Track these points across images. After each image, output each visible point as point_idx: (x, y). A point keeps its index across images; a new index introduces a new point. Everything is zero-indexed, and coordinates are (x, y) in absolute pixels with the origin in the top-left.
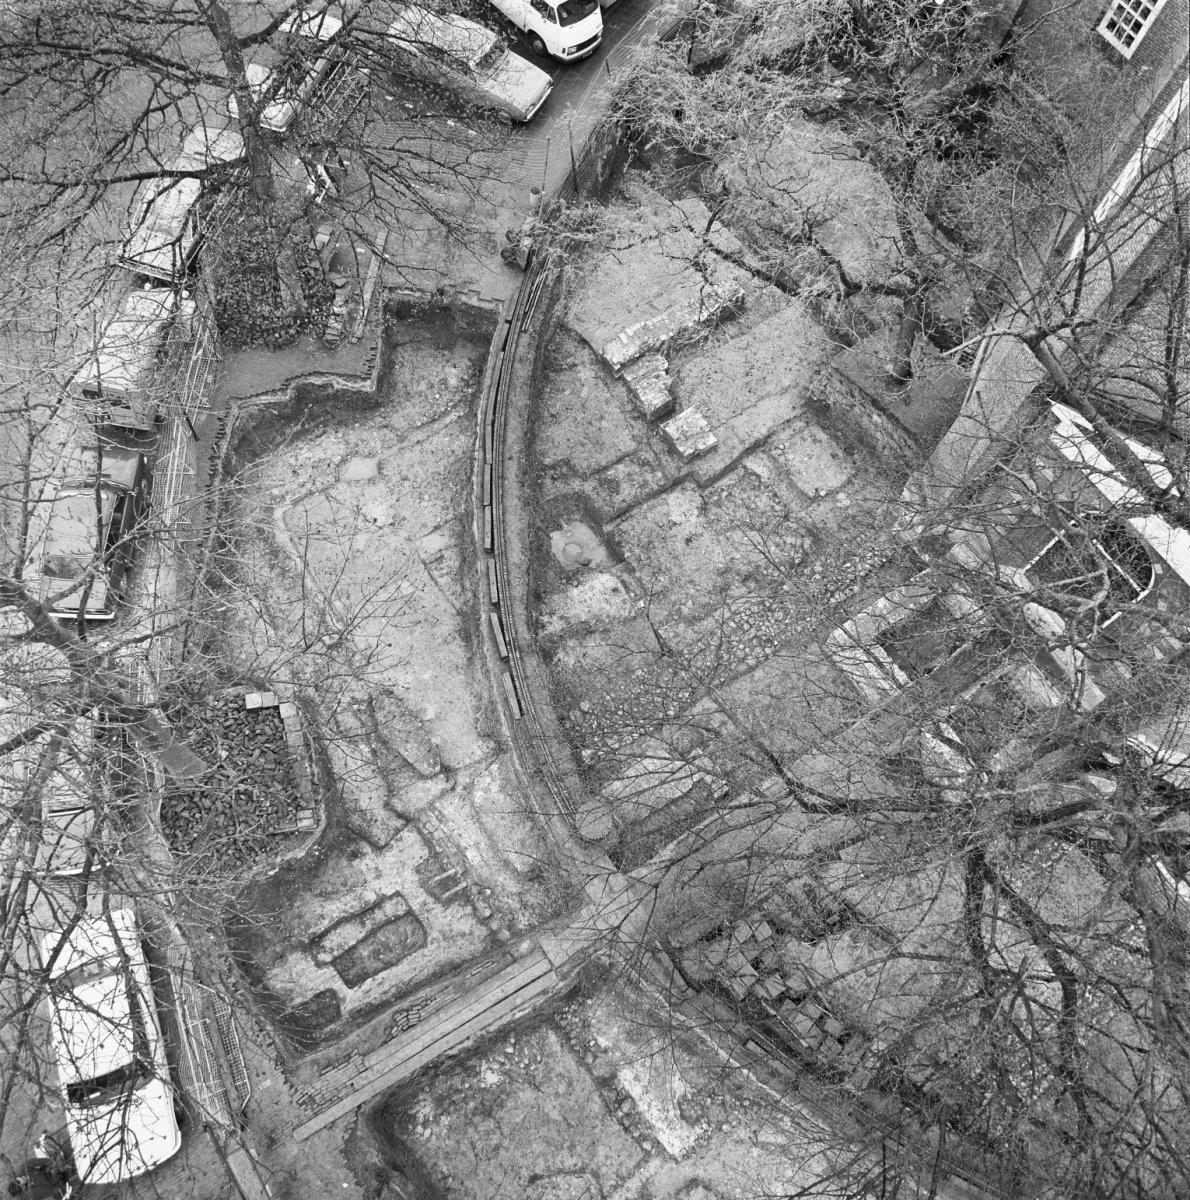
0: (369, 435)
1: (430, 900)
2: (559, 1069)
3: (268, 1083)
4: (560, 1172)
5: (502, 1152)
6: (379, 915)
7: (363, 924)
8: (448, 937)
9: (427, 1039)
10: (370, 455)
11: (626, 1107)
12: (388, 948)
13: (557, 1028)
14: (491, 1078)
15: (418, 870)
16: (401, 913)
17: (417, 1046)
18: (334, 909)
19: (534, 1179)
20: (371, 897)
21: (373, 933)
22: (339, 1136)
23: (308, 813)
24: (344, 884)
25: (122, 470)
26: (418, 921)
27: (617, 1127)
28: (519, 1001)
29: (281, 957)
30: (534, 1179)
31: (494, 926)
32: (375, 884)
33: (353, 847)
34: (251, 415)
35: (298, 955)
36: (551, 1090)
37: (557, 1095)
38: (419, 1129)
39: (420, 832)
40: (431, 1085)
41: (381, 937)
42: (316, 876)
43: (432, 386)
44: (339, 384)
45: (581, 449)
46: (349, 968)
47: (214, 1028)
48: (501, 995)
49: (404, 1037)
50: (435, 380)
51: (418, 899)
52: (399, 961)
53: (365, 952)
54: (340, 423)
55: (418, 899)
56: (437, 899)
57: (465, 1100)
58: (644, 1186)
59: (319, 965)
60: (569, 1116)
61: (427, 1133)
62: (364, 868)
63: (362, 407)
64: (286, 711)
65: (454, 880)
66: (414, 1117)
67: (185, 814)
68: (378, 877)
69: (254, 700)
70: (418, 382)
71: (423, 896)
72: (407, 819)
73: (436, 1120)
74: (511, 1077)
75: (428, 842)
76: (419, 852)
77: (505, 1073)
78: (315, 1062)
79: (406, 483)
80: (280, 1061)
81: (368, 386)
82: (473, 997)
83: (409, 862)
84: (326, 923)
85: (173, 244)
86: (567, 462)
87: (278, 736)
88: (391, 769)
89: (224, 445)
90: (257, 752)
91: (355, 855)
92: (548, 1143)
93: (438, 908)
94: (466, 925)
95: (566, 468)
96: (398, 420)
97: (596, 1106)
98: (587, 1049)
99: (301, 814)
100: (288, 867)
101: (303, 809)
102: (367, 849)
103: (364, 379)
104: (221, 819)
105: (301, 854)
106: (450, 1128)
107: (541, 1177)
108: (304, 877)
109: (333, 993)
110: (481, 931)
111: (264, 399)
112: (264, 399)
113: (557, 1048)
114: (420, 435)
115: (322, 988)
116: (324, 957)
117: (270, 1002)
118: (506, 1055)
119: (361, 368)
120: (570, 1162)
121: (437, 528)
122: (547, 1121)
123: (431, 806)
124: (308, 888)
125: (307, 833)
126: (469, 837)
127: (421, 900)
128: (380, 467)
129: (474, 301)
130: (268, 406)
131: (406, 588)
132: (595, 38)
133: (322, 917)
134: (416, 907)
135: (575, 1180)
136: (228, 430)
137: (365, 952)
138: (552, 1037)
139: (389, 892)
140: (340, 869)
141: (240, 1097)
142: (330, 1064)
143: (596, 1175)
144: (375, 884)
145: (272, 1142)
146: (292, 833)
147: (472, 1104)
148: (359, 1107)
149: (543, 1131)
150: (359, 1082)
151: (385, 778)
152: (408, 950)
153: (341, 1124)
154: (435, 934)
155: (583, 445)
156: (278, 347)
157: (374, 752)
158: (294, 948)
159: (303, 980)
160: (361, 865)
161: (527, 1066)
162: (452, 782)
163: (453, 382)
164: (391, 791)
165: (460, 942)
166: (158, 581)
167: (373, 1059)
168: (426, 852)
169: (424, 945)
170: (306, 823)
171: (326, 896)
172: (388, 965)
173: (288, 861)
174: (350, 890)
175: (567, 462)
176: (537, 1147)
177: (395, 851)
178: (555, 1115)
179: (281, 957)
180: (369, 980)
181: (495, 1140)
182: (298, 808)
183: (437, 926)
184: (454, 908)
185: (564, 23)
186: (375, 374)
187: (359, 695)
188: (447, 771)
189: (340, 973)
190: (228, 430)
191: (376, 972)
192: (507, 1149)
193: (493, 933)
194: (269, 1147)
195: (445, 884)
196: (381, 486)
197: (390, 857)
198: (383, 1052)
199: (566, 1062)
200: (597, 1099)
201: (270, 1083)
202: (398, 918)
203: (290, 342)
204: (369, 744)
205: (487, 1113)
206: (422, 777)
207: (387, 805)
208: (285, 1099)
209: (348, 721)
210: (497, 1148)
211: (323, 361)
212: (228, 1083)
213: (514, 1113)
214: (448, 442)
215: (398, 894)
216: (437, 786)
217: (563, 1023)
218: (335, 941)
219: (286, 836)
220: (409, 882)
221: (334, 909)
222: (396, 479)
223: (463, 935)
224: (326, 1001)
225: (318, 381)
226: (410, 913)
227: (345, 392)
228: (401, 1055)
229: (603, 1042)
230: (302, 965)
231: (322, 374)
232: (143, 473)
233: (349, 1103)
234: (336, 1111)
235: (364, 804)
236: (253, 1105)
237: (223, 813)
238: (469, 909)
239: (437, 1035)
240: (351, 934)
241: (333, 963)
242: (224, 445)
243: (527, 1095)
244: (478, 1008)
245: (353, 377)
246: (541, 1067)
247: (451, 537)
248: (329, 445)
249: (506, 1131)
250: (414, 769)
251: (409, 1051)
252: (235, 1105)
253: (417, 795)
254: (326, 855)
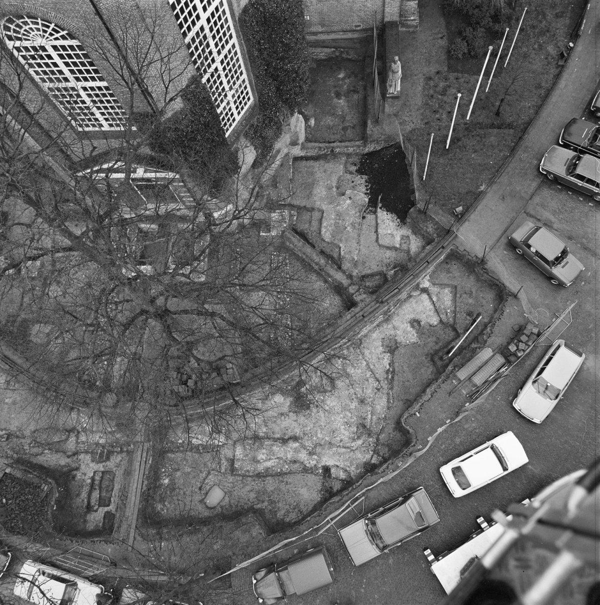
1: (104, 464)
2: (179, 459)
4: (204, 479)
5: (187, 493)
6: (97, 482)
7: (95, 489)
8: (118, 466)
12: (108, 486)
13: (168, 452)
14: (166, 481)
15: (93, 461)
17: (133, 498)
18: (84, 495)
19: (200, 489)
20: (89, 481)
21: (100, 488)
24: (80, 487)
26: (108, 471)
28: (145, 459)
30: (200, 489)
31: (125, 450)
32: (87, 477)
33: (71, 477)
35: (88, 516)
38: (162, 512)
39: (82, 453)
41: (103, 486)
47: (82, 556)
48: (139, 463)
51: (101, 467)
52: (114, 486)
55: (101, 467)
57: (166, 493)
58: (226, 458)
62: (79, 477)
66: (158, 512)
67: (12, 525)
68: (85, 475)
71: (101, 465)
72: (75, 454)
73: (164, 505)
74: (171, 475)
75: (86, 452)
78: (115, 531)
82: (133, 472)
83: (88, 462)
86: (9, 316)
88: (56, 448)
90: (12, 489)
91: (74, 477)
92: (194, 477)
93: (108, 463)
94: (119, 458)
97: (197, 456)
98: (178, 448)
99: (42, 487)
101: (41, 486)
102: (75, 472)
105: (57, 495)
106: (169, 503)
107: (202, 486)
109: (107, 512)
110: (124, 455)
113: (173, 456)
115: (103, 515)
116: (95, 508)
117: (96, 533)
118: (164, 472)
120: (204, 475)
123: (77, 443)
124: (71, 499)
133: (83, 500)
134: (102, 469)
137: (104, 494)
139: (92, 474)
140: (73, 485)
141: (108, 561)
142: (119, 527)
146: (47, 494)
150: (129, 523)
151: (60, 452)
155: (8, 307)
157: (49, 449)
158: (85, 516)
159: (97, 519)
164: (64, 452)
165: (122, 463)
168: (90, 455)
169: (115, 474)
171: (78, 495)
173: (56, 500)
174: (82, 487)
175: (9, 316)
176: (193, 481)
178: (189, 470)
179: (85, 521)
180: (112, 499)
182: (39, 487)
184: (112, 459)
187: (29, 442)
192: (187, 491)
193: (127, 451)
197: (83, 467)
198: (127, 510)
200: (194, 454)
202: (102, 477)
204: (46, 449)
206: (67, 439)
207: (69, 457)
208: (118, 547)
210: (184, 494)
215: (95, 472)
216: (73, 439)
217: (167, 449)
219: (46, 496)
220: (94, 466)
221: (84, 495)
223: (121, 461)
224: (109, 516)
226: (103, 472)
228: (132, 505)
232: (509, 344)
233: (132, 531)
234: (132, 535)
237: (20, 512)
238: (116, 454)
239: (135, 491)
240: (96, 495)
241: (99, 507)
243: (178, 474)
244: (137, 473)
249: (182, 487)
250: (62, 441)
253: (71, 444)
254: (65, 486)
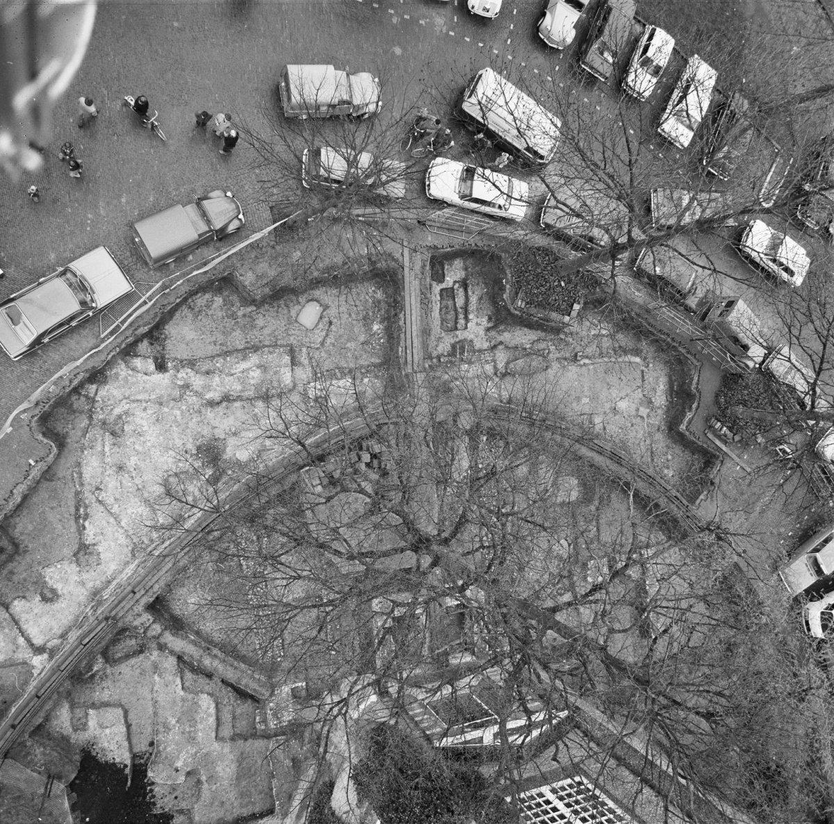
0: (658, 419)
1: (457, 340)
3: (430, 239)
4: (327, 335)
5: (348, 316)
6: (461, 316)
9: (413, 307)
10: (648, 416)
11: (339, 375)
12: (446, 313)
14: (376, 327)
15: (471, 341)
16: (458, 325)
17: (413, 302)
18: (474, 299)
19: (331, 323)
20: (471, 316)
21: (456, 310)
22: (397, 255)
23: (523, 306)
24: (481, 308)
25: (692, 302)
27: (332, 367)
29: (466, 269)
31: (434, 360)
32: (475, 321)
34: (690, 370)
36: (358, 350)
37: (355, 350)
39: (486, 350)
40: (386, 302)
42: (490, 298)
43: (668, 461)
44: (689, 415)
45: (612, 514)
46: (448, 293)
48: (414, 345)
49: (419, 299)
50: (670, 463)
51: (461, 335)
52: (440, 314)
53: (450, 303)
54: (668, 409)
55: (461, 335)
56: (457, 343)
57: (373, 312)
59: (455, 282)
60: (345, 351)
61: (370, 291)
63: (672, 427)
64: (567, 319)
65: (462, 353)
69: (576, 307)
70: (672, 455)
72: (495, 347)
76: (478, 345)
77: (374, 334)
79: (630, 425)
80: (436, 247)
81: (683, 427)
83: (158, 391)
84: (470, 293)
85: (789, 358)
87: (558, 309)
88: (517, 351)
89: (684, 351)
91: (490, 319)
94: (440, 349)
95: (604, 502)
96: (659, 436)
99: (524, 303)
100: (502, 289)
102: (490, 325)
103: (687, 427)
104: (539, 271)
105: (505, 296)
106: (367, 300)
108: (494, 297)
110: (435, 354)
111: (696, 378)
112: (696, 378)
113: (373, 360)
114: (648, 442)
118: (381, 338)
119: (693, 428)
120: (328, 341)
121: (605, 428)
122: (348, 340)
125: (513, 301)
126: (474, 370)
127: (459, 336)
128: (642, 417)
129: (702, 497)
130: (692, 379)
131: (585, 400)
132: (809, 630)
134: (457, 332)
135: (320, 339)
136: (689, 356)
138: (378, 361)
139: (469, 325)
140: (488, 309)
142: (423, 267)
143: (317, 349)
144: (475, 321)
145: (409, 230)
147: (371, 314)
148: (403, 268)
149: (346, 337)
150: (412, 273)
152: (443, 320)
153: (401, 259)
154: (443, 334)
156: (717, 396)
157: (525, 349)
158: (467, 275)
159: (452, 273)
160: (485, 319)
161: (372, 344)
162: (499, 375)
163: (666, 471)
166: (639, 295)
167: (417, 282)
168: (476, 348)
169: (441, 328)
170: (520, 303)
171: (480, 299)
172: (441, 310)
177: (483, 336)
178: (349, 345)
180: (439, 298)
181: (354, 316)
182: (527, 303)
183: (446, 337)
185: (822, 613)
186: (687, 433)
187: (551, 355)
188: (504, 375)
189: (447, 289)
190: (689, 356)
191: (441, 303)
192: (347, 319)
194: (407, 228)
195: (462, 349)
196: (634, 413)
197: (482, 333)
199: (364, 362)
201: (430, 239)
202: (456, 323)
203: (717, 402)
205: (365, 318)
207: (501, 343)
209: (542, 345)
210: (350, 315)
211: (703, 413)
212: (438, 225)
213: (358, 328)
214: (639, 454)
218: (460, 295)
219: (517, 293)
221: (474, 299)
222: (634, 421)
223: (437, 346)
224: (440, 278)
225: (694, 406)
226: (456, 329)
227: (684, 416)
229: (366, 380)
230: (459, 276)
231: (697, 409)
233: (407, 264)
235: (506, 334)
236: (425, 229)
240: (460, 301)
242: (684, 351)
243: (362, 338)
244: (414, 334)
245: (690, 422)
246: (369, 350)
247: (598, 433)
248: (660, 399)
251: (413, 297)
252: (429, 223)
253: (502, 357)
